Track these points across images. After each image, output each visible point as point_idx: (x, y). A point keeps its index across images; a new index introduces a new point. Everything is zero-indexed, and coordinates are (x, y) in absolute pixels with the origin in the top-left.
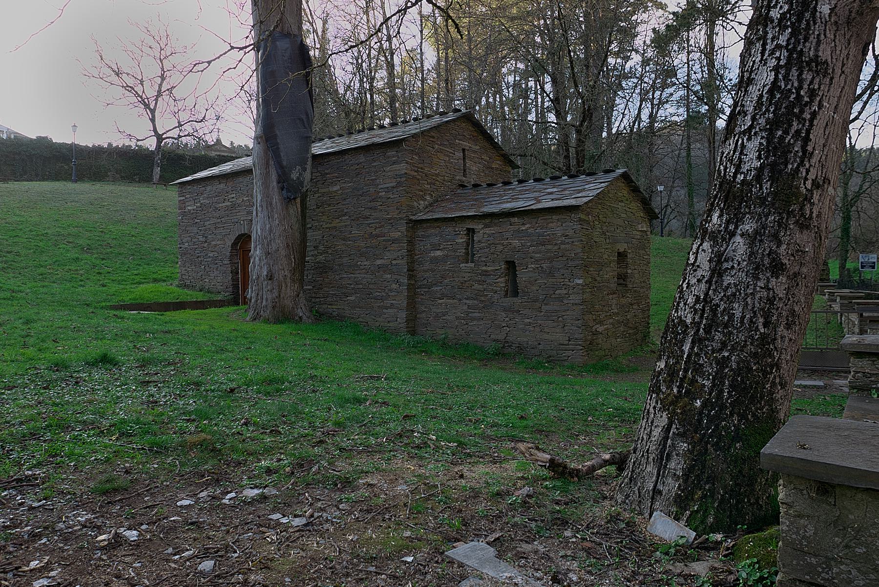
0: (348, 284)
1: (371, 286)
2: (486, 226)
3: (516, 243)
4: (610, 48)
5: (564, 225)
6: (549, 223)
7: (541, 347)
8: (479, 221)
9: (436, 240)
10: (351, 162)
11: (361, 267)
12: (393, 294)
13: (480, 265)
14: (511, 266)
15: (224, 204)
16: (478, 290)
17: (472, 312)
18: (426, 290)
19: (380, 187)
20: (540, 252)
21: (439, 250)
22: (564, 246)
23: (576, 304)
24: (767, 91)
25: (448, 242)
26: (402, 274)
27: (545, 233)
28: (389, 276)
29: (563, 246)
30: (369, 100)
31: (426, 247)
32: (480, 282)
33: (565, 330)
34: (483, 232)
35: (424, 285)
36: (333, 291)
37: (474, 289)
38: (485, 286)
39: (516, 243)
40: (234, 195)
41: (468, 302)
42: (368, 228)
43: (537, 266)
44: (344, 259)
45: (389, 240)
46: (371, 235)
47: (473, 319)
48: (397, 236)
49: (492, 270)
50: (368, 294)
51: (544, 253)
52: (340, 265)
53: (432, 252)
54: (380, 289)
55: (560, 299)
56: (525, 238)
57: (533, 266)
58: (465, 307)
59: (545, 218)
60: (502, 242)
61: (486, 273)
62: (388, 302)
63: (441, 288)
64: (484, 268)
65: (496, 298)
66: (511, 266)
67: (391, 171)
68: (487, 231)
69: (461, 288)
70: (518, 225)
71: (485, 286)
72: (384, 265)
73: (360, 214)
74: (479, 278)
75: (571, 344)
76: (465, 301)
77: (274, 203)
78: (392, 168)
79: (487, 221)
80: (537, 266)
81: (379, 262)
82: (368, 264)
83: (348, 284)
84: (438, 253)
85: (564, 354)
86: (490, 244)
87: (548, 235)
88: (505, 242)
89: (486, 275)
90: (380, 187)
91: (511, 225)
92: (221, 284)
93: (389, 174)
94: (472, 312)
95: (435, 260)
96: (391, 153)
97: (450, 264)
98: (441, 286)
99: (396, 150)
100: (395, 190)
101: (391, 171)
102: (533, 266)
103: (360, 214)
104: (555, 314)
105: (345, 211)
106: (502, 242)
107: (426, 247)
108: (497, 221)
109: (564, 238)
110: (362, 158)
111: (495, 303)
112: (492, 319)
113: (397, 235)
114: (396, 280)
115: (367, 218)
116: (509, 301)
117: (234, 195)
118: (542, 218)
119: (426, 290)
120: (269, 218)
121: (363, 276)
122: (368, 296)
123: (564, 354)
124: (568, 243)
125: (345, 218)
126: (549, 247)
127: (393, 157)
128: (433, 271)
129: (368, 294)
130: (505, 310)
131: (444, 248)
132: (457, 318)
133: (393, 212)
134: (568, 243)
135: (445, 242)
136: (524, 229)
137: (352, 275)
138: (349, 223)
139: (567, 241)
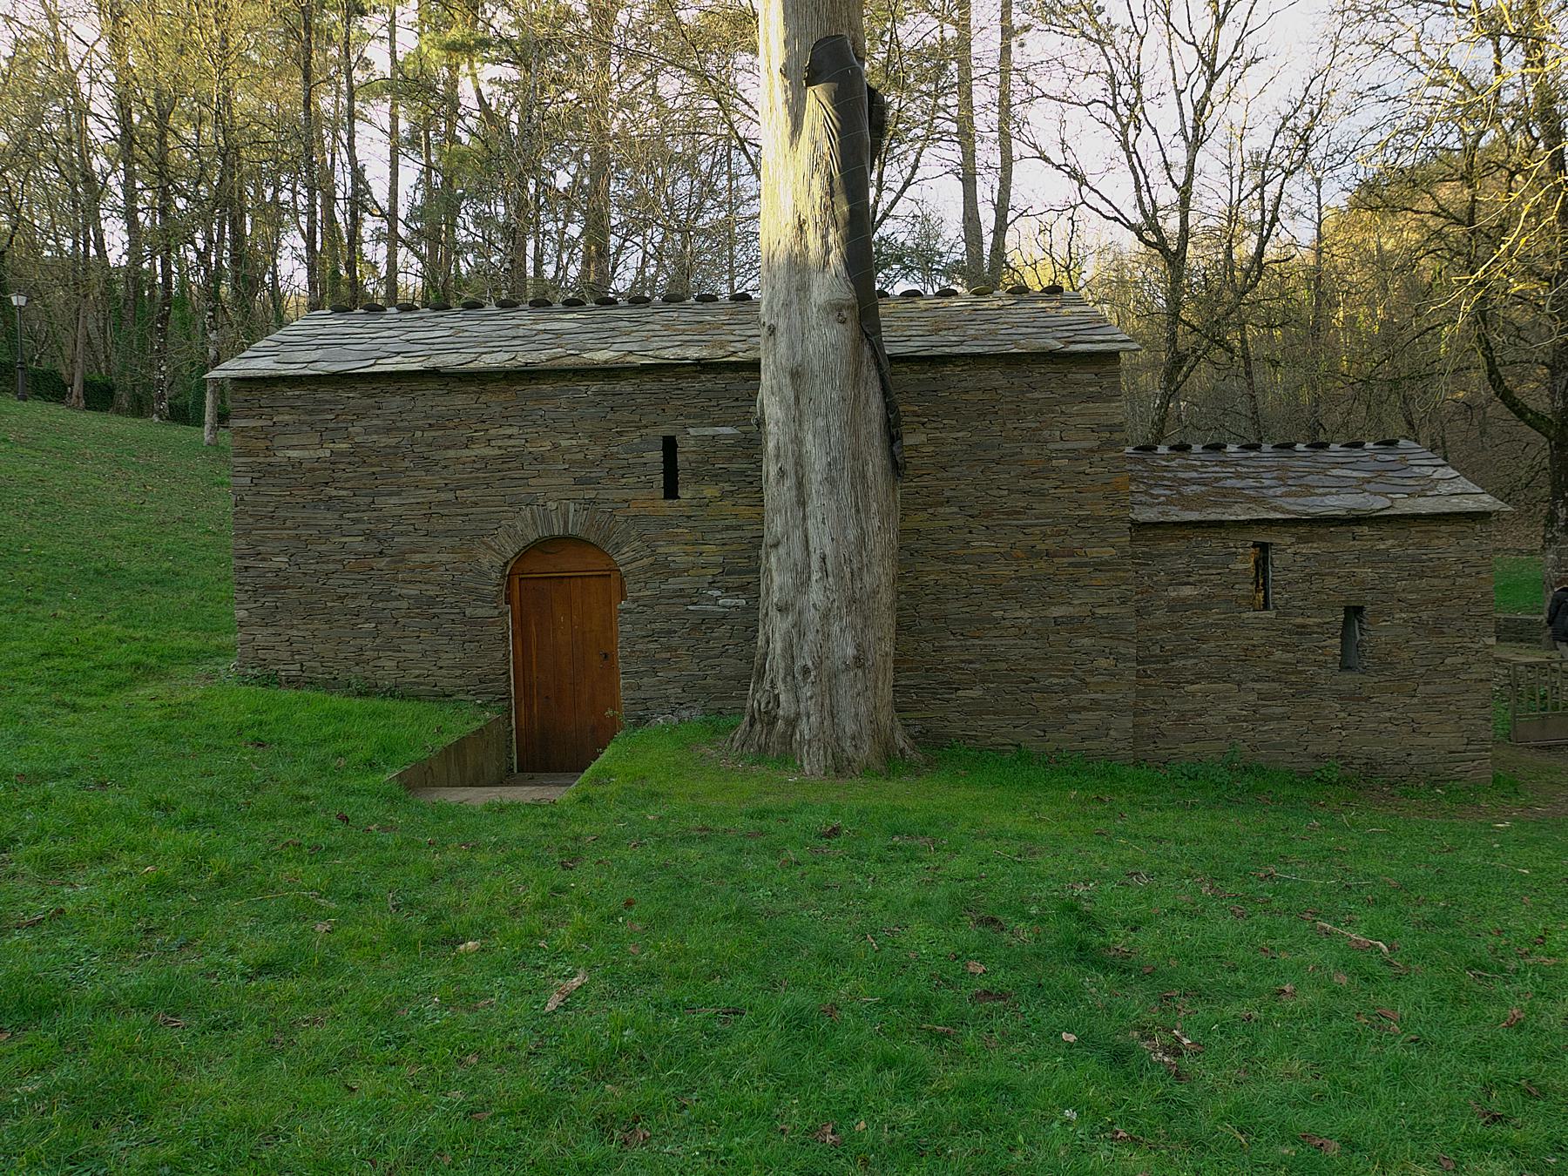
0: (962, 661)
1: (1033, 665)
2: (1301, 540)
3: (1366, 572)
4: (915, 272)
5: (1462, 543)
6: (1433, 539)
7: (1413, 760)
8: (1283, 529)
9: (1180, 564)
10: (964, 384)
11: (1007, 623)
12: (1101, 679)
13: (1289, 614)
14: (1354, 612)
15: (466, 452)
16: (1284, 664)
17: (1264, 706)
18: (1159, 666)
19: (1052, 446)
20: (1418, 591)
21: (1189, 584)
22: (1462, 580)
23: (1481, 680)
24: (760, 364)
25: (1209, 568)
26: (1123, 636)
27: (1424, 557)
28: (1086, 641)
29: (1460, 581)
30: (531, 273)
31: (1155, 579)
32: (1286, 648)
33: (1461, 727)
34: (1288, 552)
35: (1152, 656)
36: (908, 678)
37: (1275, 661)
38: (1299, 655)
39: (1366, 572)
40: (514, 431)
41: (1258, 686)
42: (1021, 536)
43: (1412, 615)
44: (949, 606)
45: (1086, 565)
46: (1032, 553)
47: (1267, 719)
48: (1106, 557)
49: (1318, 625)
50: (1023, 682)
51: (1425, 593)
52: (934, 619)
53: (1170, 588)
54: (1061, 670)
55: (1453, 673)
56: (1385, 565)
57: (1404, 615)
58: (1252, 698)
59: (1423, 528)
60: (1337, 570)
61: (1302, 630)
62: (1083, 698)
63: (1196, 661)
64: (1299, 620)
65: (1323, 676)
66: (1354, 612)
67: (1084, 415)
68: (1305, 549)
69: (1242, 660)
70: (1370, 540)
71: (1299, 655)
72: (1072, 618)
73: (992, 503)
74: (1287, 639)
75: (1470, 751)
76: (1251, 685)
77: (870, 473)
78: (1088, 408)
79: (1302, 530)
80: (1412, 615)
81: (1057, 611)
82: (1027, 615)
83: (962, 661)
84: (1187, 591)
85: (1458, 769)
86: (1311, 576)
87: (1431, 560)
88: (1343, 572)
89: (1302, 633)
90: (1052, 446)
91: (1354, 539)
92: (459, 672)
93: (1079, 420)
94: (1264, 706)
95: (1175, 606)
96: (1084, 376)
97: (1217, 613)
98: (1195, 657)
99: (1096, 371)
100: (1097, 457)
101: (1084, 415)
102: (1404, 615)
103: (992, 503)
104: (1444, 699)
105: (948, 493)
106: (1337, 570)
107: (1155, 579)
108: (1322, 531)
109: (1461, 566)
110: (997, 378)
111: (1319, 686)
112: (1310, 716)
113: (1107, 553)
114: (1107, 650)
115: (1019, 513)
116: (1348, 680)
117: (514, 431)
118: (1418, 529)
119: (1159, 666)
120: (858, 511)
121: (1012, 642)
122: (1023, 686)
123: (1458, 769)
124: (1470, 575)
125: (948, 510)
126: (1436, 582)
127: (1090, 384)
128: (1174, 626)
129: (1023, 682)
130: (1341, 697)
131: (1201, 582)
132: (1231, 719)
133: (1092, 504)
134: (1470, 575)
135: (1202, 568)
136: (1383, 547)
137: (977, 642)
138: (961, 522)
139: (1467, 571)
